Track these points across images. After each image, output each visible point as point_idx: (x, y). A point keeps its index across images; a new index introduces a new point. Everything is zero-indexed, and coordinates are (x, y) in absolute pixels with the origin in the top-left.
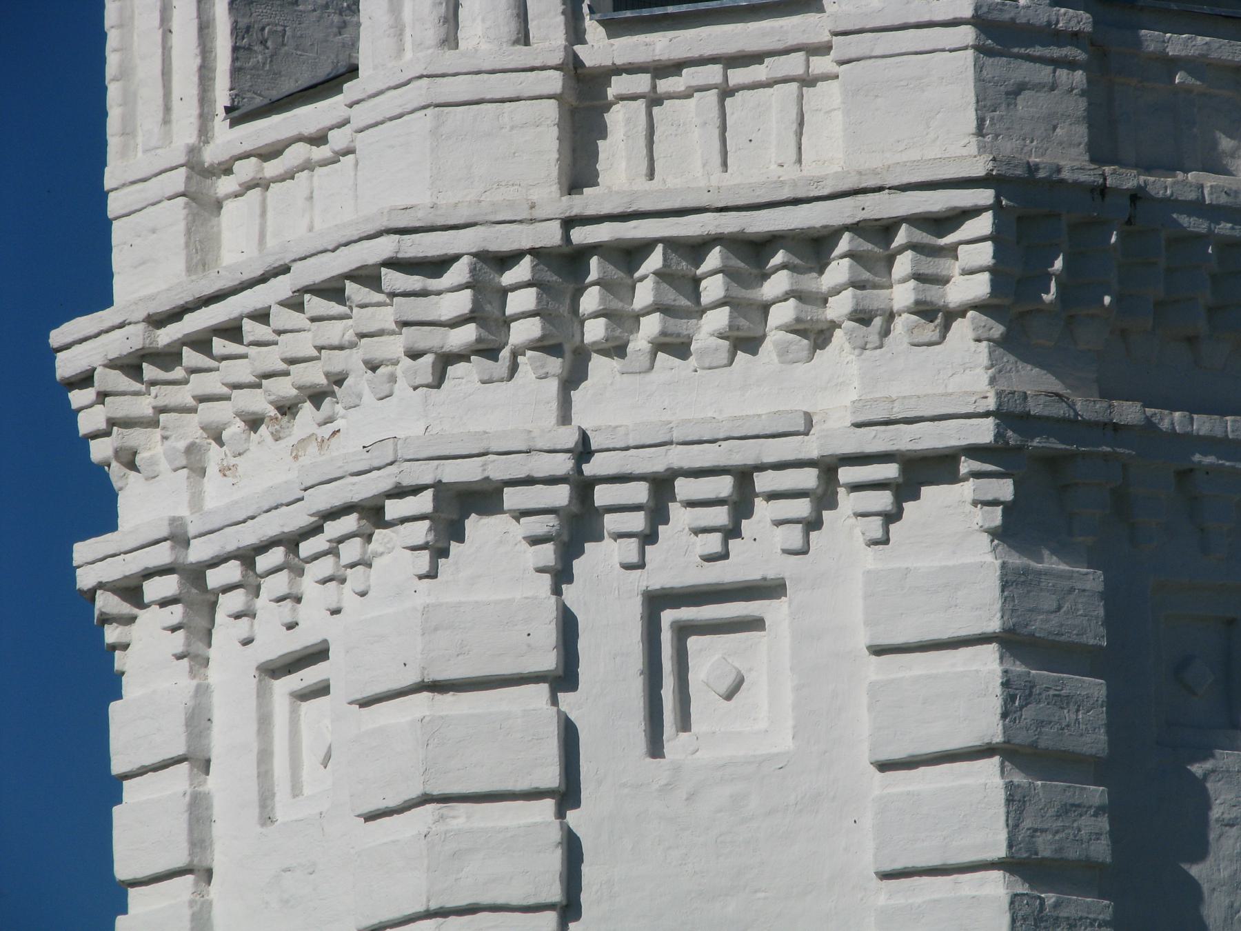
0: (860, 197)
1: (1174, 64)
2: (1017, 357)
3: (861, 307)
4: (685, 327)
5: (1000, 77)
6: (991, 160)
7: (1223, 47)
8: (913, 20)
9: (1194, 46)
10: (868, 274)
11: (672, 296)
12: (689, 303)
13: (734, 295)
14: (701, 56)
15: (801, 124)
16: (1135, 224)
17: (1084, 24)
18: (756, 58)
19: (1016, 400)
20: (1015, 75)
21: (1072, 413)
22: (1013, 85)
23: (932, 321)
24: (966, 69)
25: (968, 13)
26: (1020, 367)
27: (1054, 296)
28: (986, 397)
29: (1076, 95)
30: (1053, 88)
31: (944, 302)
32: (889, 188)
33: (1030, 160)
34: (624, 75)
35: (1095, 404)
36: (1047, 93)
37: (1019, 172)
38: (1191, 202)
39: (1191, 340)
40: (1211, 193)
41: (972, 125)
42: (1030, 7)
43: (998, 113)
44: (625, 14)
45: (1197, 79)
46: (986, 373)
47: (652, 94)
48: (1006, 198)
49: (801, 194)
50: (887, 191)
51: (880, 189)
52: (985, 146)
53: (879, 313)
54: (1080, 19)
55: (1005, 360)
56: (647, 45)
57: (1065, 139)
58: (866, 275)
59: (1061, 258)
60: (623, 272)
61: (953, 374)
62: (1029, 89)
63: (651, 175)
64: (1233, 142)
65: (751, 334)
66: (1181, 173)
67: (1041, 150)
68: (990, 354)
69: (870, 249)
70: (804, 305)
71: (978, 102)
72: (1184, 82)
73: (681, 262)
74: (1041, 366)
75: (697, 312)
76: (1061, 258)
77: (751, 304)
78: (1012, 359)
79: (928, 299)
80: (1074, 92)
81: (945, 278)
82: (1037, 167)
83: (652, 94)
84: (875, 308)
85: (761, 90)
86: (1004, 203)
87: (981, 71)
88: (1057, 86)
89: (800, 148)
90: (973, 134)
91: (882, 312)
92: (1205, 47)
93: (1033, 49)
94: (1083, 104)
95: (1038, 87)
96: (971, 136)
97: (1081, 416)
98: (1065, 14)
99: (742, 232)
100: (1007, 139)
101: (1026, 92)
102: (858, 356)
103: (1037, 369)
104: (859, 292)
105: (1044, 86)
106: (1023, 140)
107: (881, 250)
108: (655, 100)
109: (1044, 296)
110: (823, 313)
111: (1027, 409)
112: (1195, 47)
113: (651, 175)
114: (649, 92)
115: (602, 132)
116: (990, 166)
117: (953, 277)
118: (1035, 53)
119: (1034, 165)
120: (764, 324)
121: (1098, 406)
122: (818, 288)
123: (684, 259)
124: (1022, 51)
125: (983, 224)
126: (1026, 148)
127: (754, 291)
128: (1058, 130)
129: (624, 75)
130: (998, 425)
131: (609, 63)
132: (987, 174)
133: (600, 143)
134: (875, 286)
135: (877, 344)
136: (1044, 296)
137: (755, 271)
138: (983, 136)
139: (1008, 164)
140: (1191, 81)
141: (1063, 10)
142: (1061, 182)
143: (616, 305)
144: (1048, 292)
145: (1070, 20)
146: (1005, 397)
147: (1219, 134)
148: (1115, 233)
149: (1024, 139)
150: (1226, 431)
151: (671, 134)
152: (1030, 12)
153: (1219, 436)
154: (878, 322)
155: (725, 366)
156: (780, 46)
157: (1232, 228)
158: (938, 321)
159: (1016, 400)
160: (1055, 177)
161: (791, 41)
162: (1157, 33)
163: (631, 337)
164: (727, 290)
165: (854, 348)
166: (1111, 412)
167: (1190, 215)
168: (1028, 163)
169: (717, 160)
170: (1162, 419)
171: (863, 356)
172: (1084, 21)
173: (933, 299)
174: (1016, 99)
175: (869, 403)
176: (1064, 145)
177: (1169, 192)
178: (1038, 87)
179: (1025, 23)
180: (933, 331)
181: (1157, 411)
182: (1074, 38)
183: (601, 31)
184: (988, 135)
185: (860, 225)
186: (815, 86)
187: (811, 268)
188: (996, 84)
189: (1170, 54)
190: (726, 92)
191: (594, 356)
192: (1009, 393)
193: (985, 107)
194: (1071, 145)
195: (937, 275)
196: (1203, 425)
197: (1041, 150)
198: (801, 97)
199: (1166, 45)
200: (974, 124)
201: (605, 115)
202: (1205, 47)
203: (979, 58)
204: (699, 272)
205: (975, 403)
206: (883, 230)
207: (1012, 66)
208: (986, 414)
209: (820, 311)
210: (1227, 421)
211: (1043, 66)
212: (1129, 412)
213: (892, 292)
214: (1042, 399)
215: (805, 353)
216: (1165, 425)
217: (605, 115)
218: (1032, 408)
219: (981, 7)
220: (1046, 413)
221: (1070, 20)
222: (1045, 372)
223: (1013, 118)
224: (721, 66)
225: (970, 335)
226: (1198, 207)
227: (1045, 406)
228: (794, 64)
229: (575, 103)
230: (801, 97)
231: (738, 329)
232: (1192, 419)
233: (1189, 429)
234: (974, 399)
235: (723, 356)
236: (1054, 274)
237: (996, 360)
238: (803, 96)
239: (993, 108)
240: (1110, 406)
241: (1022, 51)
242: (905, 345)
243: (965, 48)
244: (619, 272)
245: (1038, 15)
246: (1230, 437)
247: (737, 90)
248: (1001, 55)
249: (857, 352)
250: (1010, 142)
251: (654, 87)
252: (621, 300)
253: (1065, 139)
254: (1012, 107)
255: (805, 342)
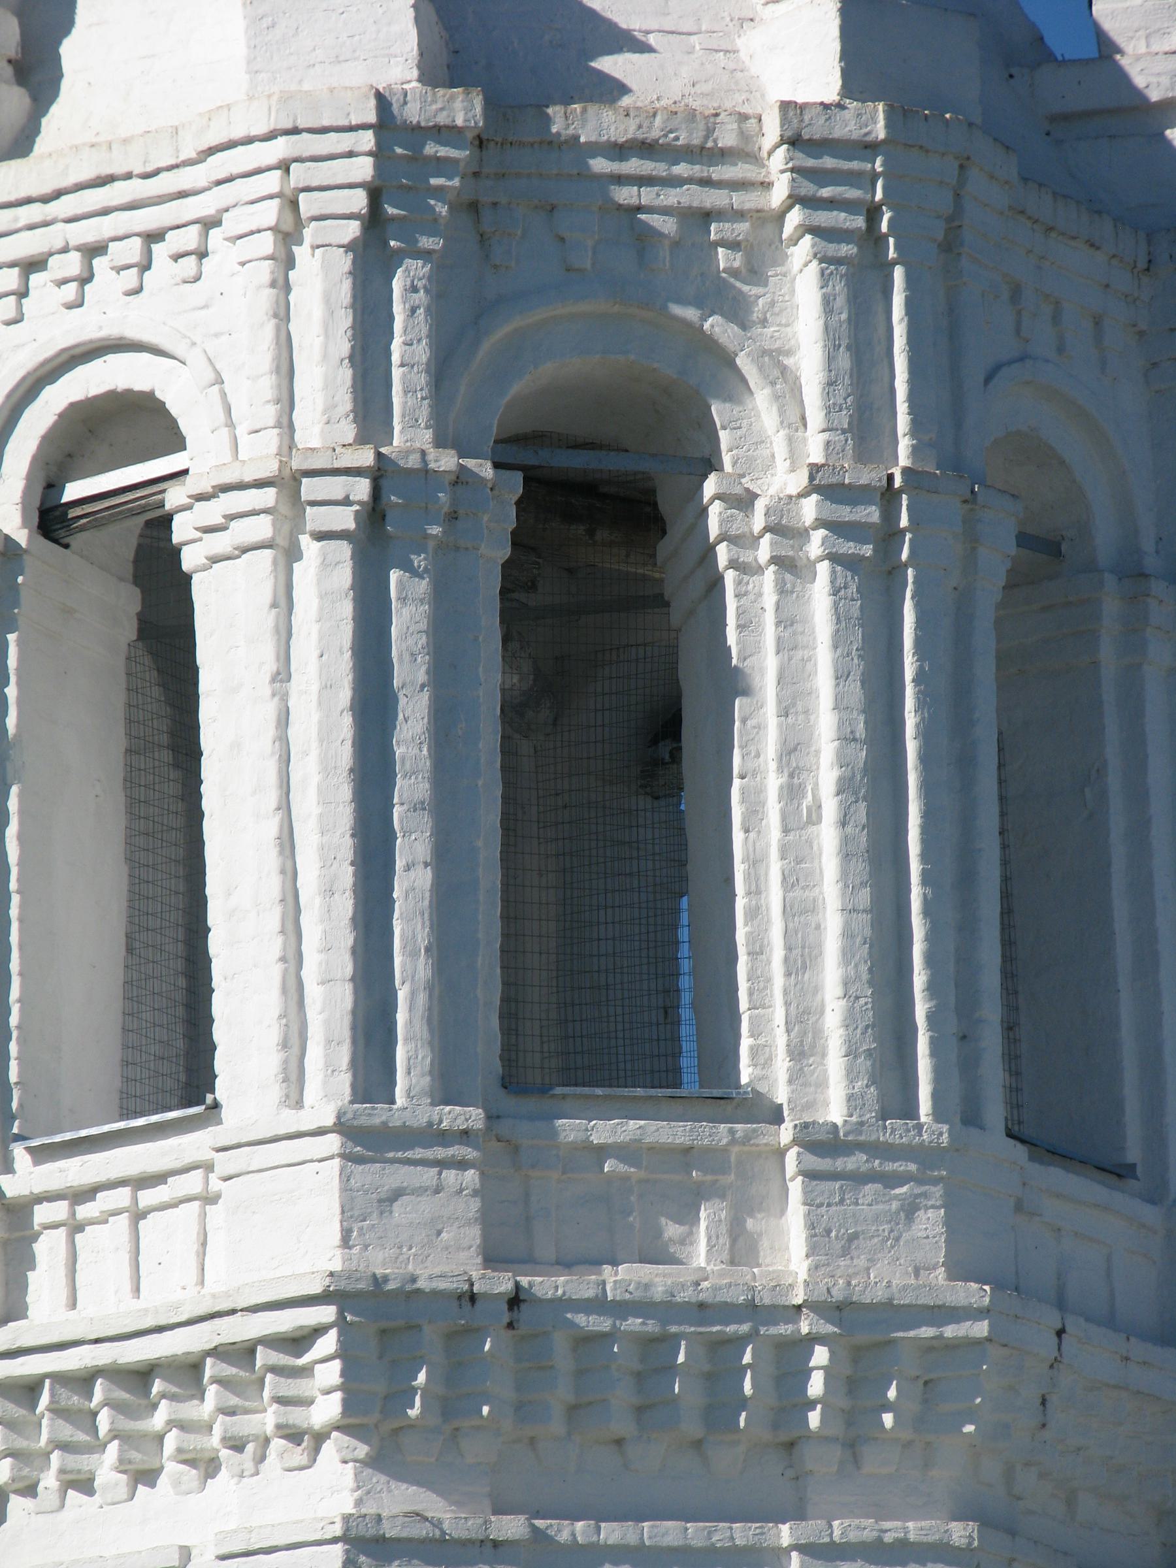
0: (217, 1321)
1: (602, 1152)
2: (388, 1475)
3: (230, 1435)
4: (86, 1463)
5: (371, 1184)
6: (328, 1276)
7: (661, 1130)
8: (282, 1131)
9: (625, 1131)
10: (238, 1399)
11: (68, 1432)
12: (89, 1438)
13: (121, 1428)
14: (108, 1180)
15: (204, 1244)
16: (518, 1329)
17: (473, 1121)
18: (159, 1179)
19: (367, 1524)
20: (390, 1181)
21: (438, 1533)
22: (387, 1191)
23: (299, 1445)
24: (332, 1179)
25: (329, 1121)
26: (393, 1486)
27: (419, 1411)
28: (333, 1523)
29: (466, 1195)
30: (437, 1190)
31: (309, 1424)
32: (241, 1310)
33: (377, 1272)
34: (45, 1203)
35: (466, 1521)
36: (430, 1197)
37: (361, 1286)
38: (588, 1300)
39: (619, 1442)
40: (614, 1289)
41: (336, 1236)
42: (407, 1108)
43: (368, 1222)
44: (126, 1125)
45: (631, 1166)
46: (352, 1495)
47: (71, 1221)
48: (349, 1313)
49: (163, 1321)
50: (240, 1313)
51: (233, 1312)
52: (351, 1259)
53: (251, 1438)
54: (468, 1117)
55: (374, 1480)
56: (60, 1171)
57: (452, 1243)
58: (234, 1401)
59: (424, 1370)
60: (25, 1409)
61: (322, 1499)
62: (408, 1194)
63: (73, 1304)
64: (682, 1227)
65: (146, 1466)
66: (610, 1267)
67: (421, 1257)
68: (356, 1475)
69: (234, 1373)
70: (186, 1435)
71: (343, 1212)
72: (613, 1171)
73: (72, 1397)
74: (418, 1483)
75: (99, 1446)
76: (424, 1370)
77: (145, 1435)
78: (383, 1478)
79: (291, 1422)
80: (464, 1193)
81: (309, 1400)
82: (386, 1279)
83: (71, 1221)
84: (246, 1434)
85: (170, 1210)
86: (348, 1319)
87: (348, 1180)
88: (443, 1188)
89: (203, 1269)
90: (338, 1247)
91: (256, 1438)
92: (638, 1132)
93: (412, 1152)
94: (475, 1204)
95: (420, 1191)
96: (337, 1249)
97: (450, 1535)
98: (450, 1113)
99: (115, 1362)
100: (378, 1249)
101: (404, 1197)
102: (237, 1484)
103: (415, 1488)
104: (228, 1418)
105: (426, 1190)
106: (399, 1248)
107: (247, 1374)
108: (77, 1228)
109: (409, 1412)
110: (209, 1441)
111: (381, 1532)
112: (625, 1133)
113: (73, 1304)
114: (68, 1219)
115: (31, 1264)
116: (327, 1281)
117: (316, 1397)
118: (414, 1157)
119: (381, 1277)
120: (160, 1454)
121: (470, 1523)
122: (200, 1416)
123: (76, 1394)
124: (399, 1155)
125: (328, 1343)
126: (401, 1257)
127: (144, 1422)
128: (444, 1235)
129: (45, 1203)
130: (347, 1552)
131: (27, 1193)
132: (324, 1291)
133: (29, 1274)
134: (247, 1411)
135: (252, 1471)
136: (409, 1412)
137: (144, 1402)
138: (350, 1248)
139: (349, 1278)
140: (622, 1168)
141: (448, 1108)
142: (417, 1292)
143: (21, 1443)
144: (412, 1407)
145: (455, 1119)
146: (353, 1522)
147: (663, 1220)
148: (489, 1339)
149: (400, 1247)
150: (642, 1538)
151: (91, 1262)
152: (407, 1113)
153: (632, 1544)
154: (250, 1447)
155: (126, 1501)
156: (177, 1165)
157: (643, 1324)
158: (305, 1444)
159: (367, 1524)
160: (408, 1287)
161: (188, 1160)
162: (578, 1121)
163: (42, 1476)
164: (112, 1423)
165: (233, 1477)
166: (486, 1529)
167: (588, 1314)
168: (374, 1275)
169: (127, 1286)
170: (559, 1531)
171: (241, 1485)
172: (473, 1118)
173: (296, 1422)
174: (391, 1206)
175: (229, 1535)
176: (450, 1250)
177: (560, 1292)
178: (420, 1191)
179: (399, 1126)
180: (302, 1455)
181: (553, 1522)
182: (465, 1136)
183: (28, 1158)
184: (357, 1245)
185: (219, 1349)
186: (216, 1203)
187: (193, 1395)
188: (366, 1192)
189: (595, 1142)
190: (138, 1216)
191: (12, 1497)
192: (358, 1517)
193: (352, 1217)
194: (459, 1249)
195: (298, 1396)
196: (612, 1533)
197: (421, 1257)
198: (203, 1215)
199: (589, 1133)
200: (339, 1236)
201: (33, 1245)
202: (638, 1132)
203: (347, 1166)
204: (93, 1405)
205: (322, 1529)
206: (243, 1353)
207: (387, 1172)
208: (334, 1541)
209: (206, 1439)
210: (643, 1527)
211: (426, 1169)
212: (511, 1527)
213: (265, 1416)
214: (401, 1520)
215: (195, 1484)
216: (564, 1537)
217: (33, 1245)
218: (387, 1531)
219: (345, 1113)
220: (404, 1534)
221: (455, 1119)
222: (424, 1490)
223: (387, 1226)
224: (130, 1188)
225: (336, 1458)
226: (599, 1305)
227: (403, 1527)
228: (192, 1183)
229: (6, 1236)
230: (203, 1215)
231: (130, 1462)
232: (598, 1529)
233: (595, 1539)
234: (322, 1525)
235: (123, 1491)
236: (419, 1388)
237: (364, 1482)
238: (206, 1214)
239: (361, 1218)
240: (486, 1522)
241: (399, 1155)
242: (279, 1471)
243: (332, 1157)
244: (20, 1410)
245: (416, 1116)
246: (647, 1543)
247: (149, 1212)
248: (373, 1161)
249: (236, 1479)
250: (381, 1252)
251: (135, 1200)
252: (27, 1439)
253: (452, 1243)
254: (386, 1214)
255: (194, 1472)
